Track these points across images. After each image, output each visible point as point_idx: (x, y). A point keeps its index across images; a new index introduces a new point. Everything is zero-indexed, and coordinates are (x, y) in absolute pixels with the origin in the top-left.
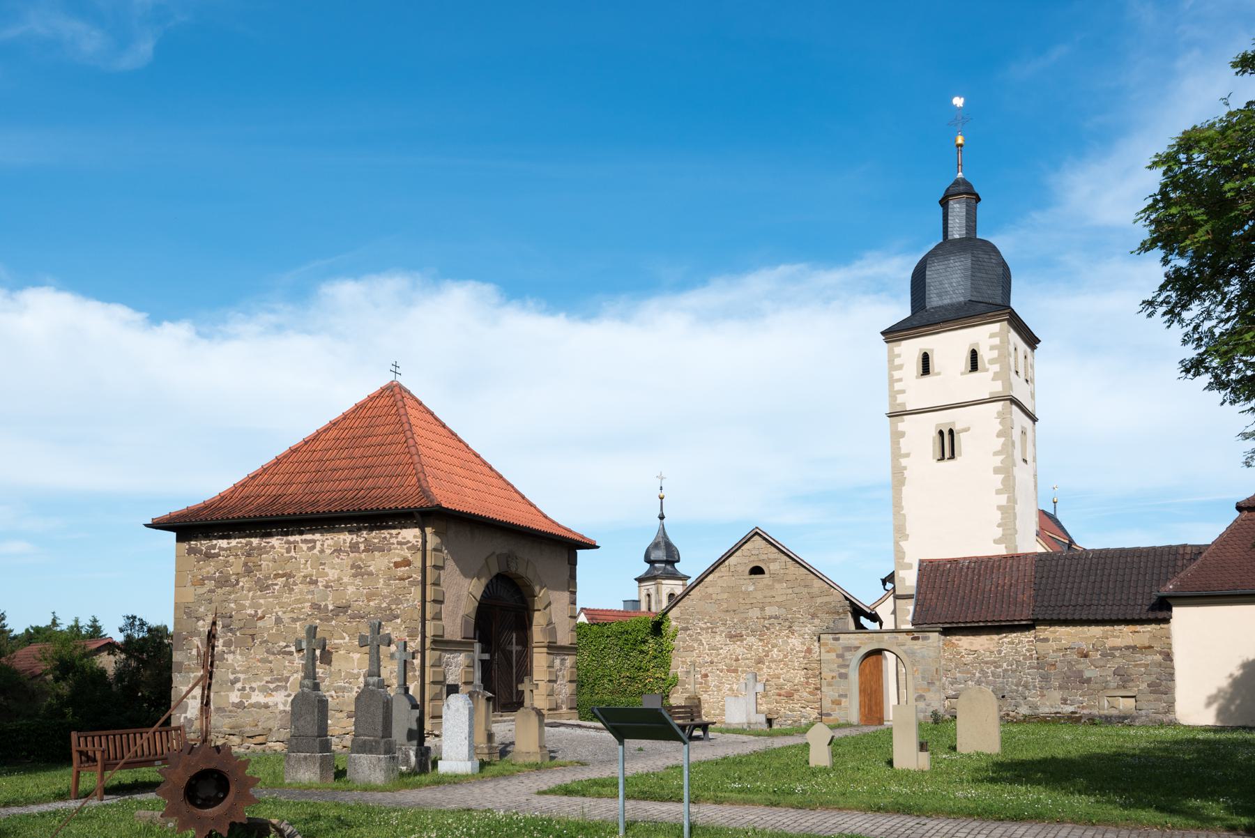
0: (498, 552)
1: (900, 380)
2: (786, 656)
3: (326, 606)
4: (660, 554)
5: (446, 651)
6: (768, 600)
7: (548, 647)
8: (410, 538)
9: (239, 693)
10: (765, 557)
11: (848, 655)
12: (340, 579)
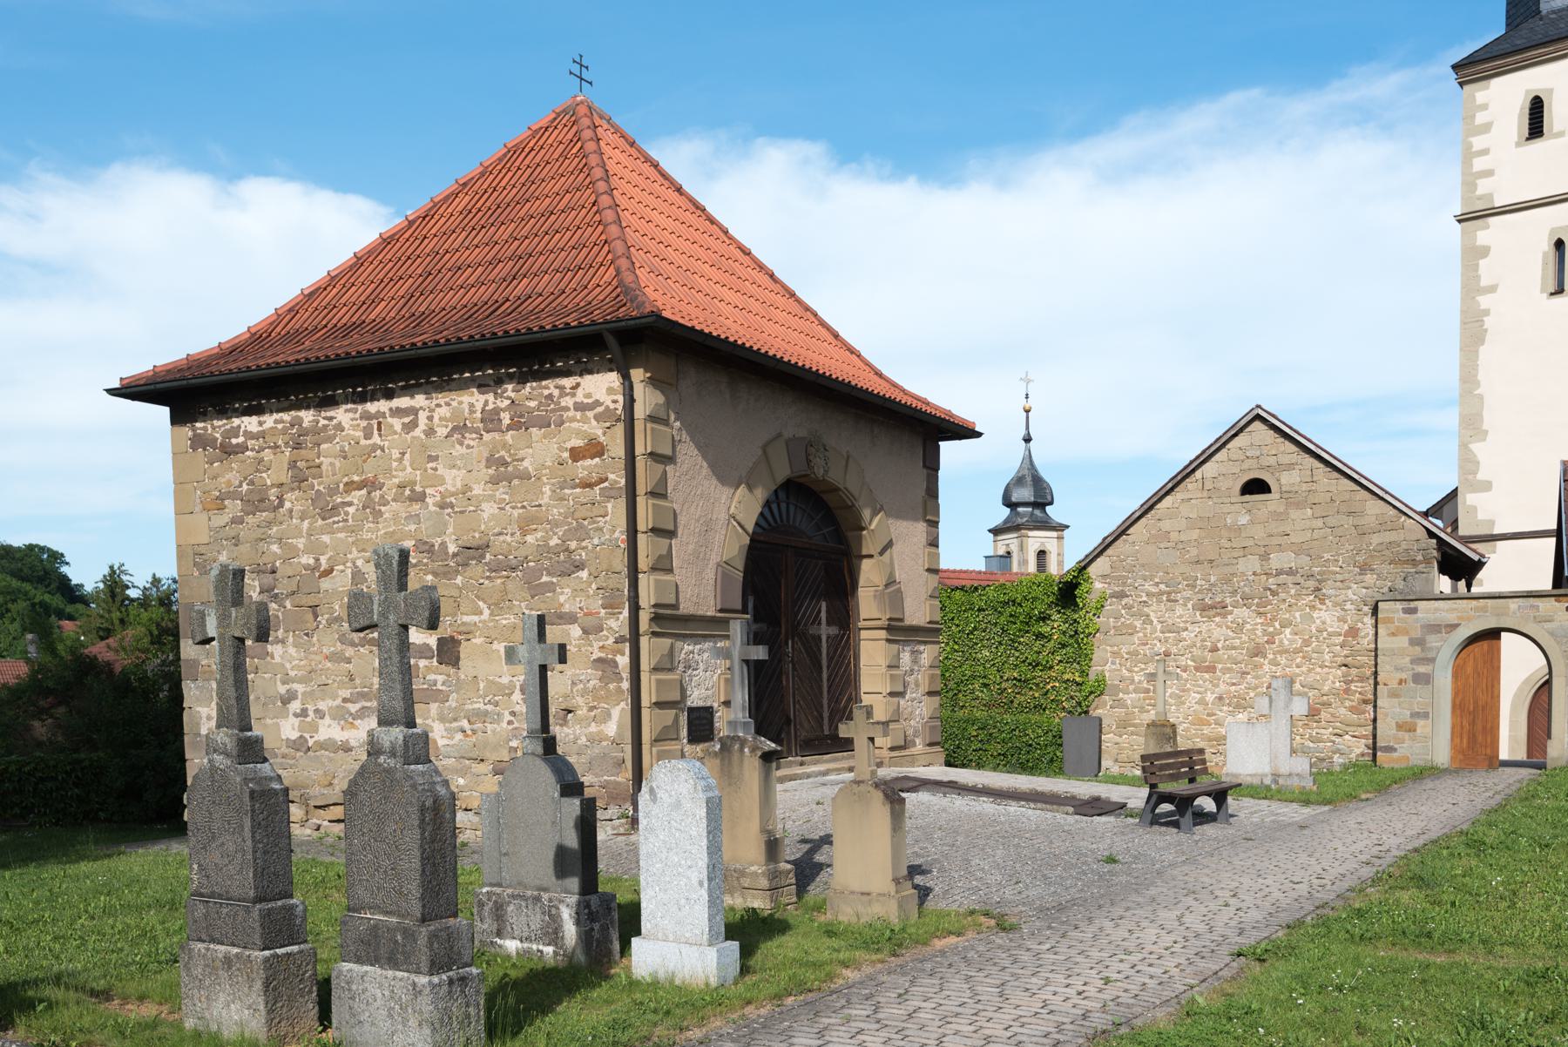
0: (788, 434)
1: (1485, 152)
2: (1307, 643)
3: (443, 544)
4: (1024, 494)
5: (684, 637)
6: (1275, 541)
7: (889, 629)
8: (601, 395)
9: (296, 721)
10: (1272, 461)
11: (1433, 640)
12: (467, 488)
